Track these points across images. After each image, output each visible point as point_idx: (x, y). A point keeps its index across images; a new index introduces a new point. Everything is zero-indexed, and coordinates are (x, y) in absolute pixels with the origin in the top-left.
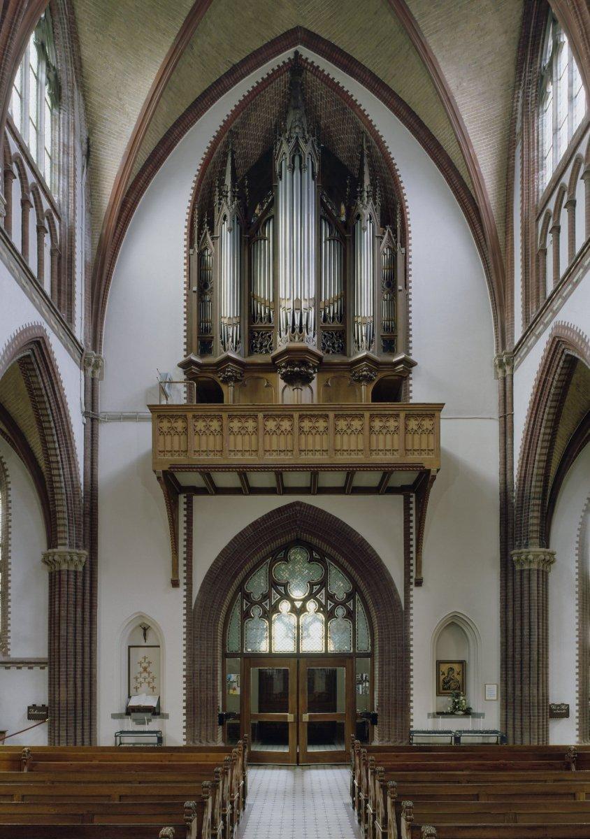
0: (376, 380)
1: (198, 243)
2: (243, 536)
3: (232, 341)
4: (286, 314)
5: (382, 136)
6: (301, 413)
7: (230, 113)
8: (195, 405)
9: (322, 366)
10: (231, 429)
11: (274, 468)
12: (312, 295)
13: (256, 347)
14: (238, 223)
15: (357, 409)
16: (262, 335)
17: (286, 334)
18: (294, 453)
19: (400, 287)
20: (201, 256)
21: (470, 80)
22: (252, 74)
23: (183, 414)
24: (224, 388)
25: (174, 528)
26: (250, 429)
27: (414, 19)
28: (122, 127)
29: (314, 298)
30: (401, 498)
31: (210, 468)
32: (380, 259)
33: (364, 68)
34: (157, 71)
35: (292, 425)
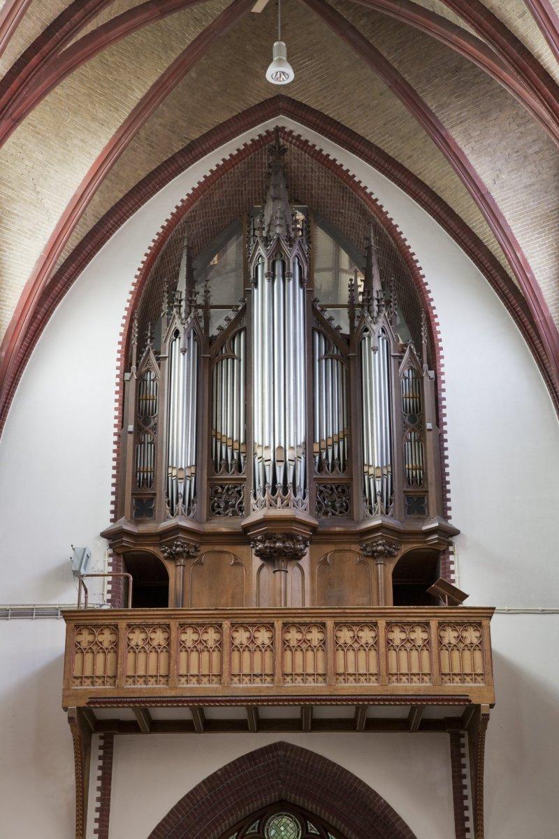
0: (399, 555)
1: (137, 365)
2: (192, 801)
3: (184, 503)
4: (264, 467)
5: (397, 226)
6: (285, 620)
7: (185, 198)
8: (131, 611)
9: (317, 536)
10: (182, 644)
11: (246, 701)
12: (301, 438)
13: (219, 506)
14: (194, 340)
15: (367, 615)
16: (228, 490)
17: (264, 495)
18: (276, 678)
19: (429, 426)
20: (141, 381)
21: (512, 171)
22: (216, 150)
23: (113, 622)
24: (171, 568)
25: (83, 774)
26: (211, 644)
27: (430, 111)
28: (37, 224)
29: (305, 443)
30: (446, 736)
31: (149, 702)
32: (399, 387)
33: (369, 144)
34: (90, 165)
35: (272, 638)
